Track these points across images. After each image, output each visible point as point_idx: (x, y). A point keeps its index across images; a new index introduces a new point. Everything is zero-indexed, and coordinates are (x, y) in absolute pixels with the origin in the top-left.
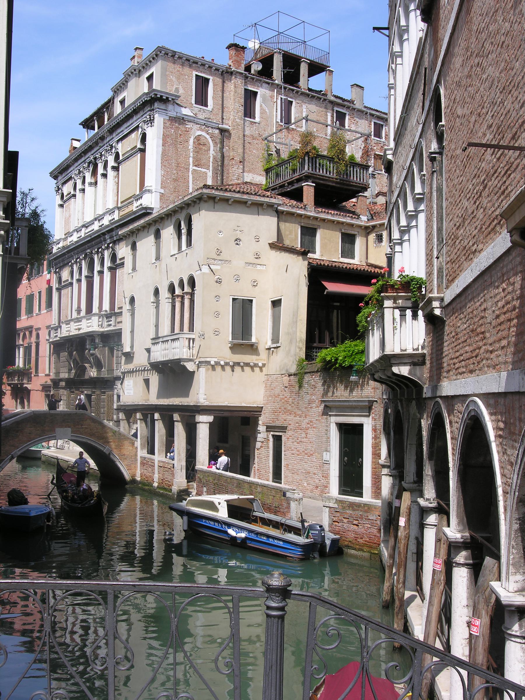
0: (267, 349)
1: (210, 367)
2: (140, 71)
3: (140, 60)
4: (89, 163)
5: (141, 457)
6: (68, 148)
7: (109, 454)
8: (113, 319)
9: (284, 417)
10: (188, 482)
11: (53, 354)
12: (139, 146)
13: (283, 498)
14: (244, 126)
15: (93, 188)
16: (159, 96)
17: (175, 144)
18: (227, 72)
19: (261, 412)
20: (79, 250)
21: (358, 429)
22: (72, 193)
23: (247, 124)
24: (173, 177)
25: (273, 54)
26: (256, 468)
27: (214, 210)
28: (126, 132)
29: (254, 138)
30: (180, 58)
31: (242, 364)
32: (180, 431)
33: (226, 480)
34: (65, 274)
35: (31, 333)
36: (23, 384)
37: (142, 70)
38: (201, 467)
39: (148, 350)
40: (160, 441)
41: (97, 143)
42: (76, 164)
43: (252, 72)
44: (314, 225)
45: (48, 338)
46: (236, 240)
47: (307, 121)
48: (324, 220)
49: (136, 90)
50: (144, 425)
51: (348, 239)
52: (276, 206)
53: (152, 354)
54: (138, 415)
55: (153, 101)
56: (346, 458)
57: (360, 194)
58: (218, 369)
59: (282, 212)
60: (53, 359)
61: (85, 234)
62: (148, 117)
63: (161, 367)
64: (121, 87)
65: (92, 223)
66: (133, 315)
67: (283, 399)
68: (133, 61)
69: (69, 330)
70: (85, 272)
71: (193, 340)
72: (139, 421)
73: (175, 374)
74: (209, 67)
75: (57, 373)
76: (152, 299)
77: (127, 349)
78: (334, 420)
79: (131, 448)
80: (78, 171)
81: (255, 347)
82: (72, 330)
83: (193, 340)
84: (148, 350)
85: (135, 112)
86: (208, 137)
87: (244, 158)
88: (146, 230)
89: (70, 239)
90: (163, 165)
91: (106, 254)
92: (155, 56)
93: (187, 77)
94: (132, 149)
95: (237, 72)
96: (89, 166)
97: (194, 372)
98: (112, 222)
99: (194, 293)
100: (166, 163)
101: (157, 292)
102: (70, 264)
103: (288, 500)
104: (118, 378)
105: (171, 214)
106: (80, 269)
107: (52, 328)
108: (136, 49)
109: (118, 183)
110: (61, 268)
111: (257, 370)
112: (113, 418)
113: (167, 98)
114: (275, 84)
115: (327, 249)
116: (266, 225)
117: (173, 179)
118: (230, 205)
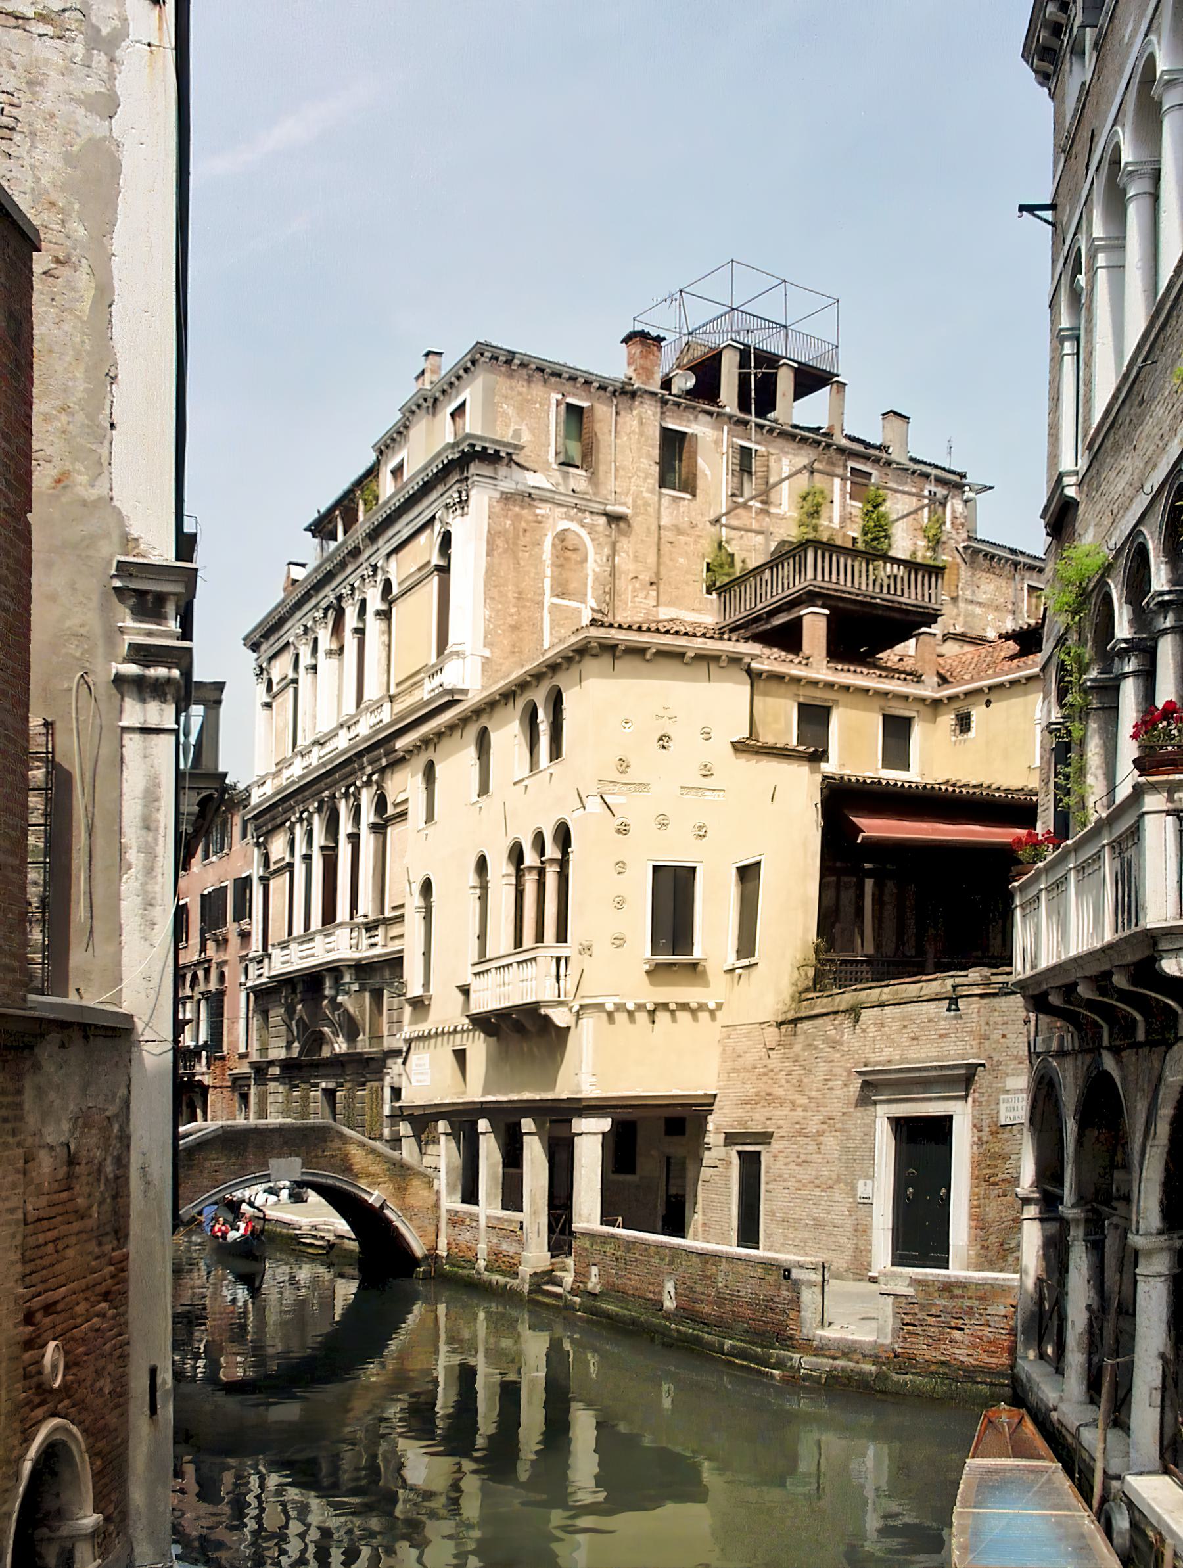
0: (725, 971)
1: (604, 1016)
2: (436, 400)
3: (435, 378)
4: (326, 609)
5: (448, 1211)
6: (281, 582)
7: (382, 1207)
8: (380, 931)
9: (766, 1112)
10: (552, 1257)
11: (254, 1012)
12: (436, 560)
13: (784, 1282)
14: (659, 505)
15: (334, 661)
16: (478, 448)
17: (512, 550)
18: (623, 392)
19: (712, 1104)
20: (307, 793)
21: (941, 1128)
22: (291, 675)
23: (665, 501)
24: (510, 621)
25: (720, 353)
26: (700, 1222)
27: (613, 674)
28: (405, 534)
29: (679, 531)
30: (523, 365)
31: (672, 1006)
32: (534, 1153)
33: (646, 1250)
34: (278, 847)
35: (207, 971)
36: (194, 1075)
37: (441, 398)
38: (585, 1225)
39: (465, 991)
40: (492, 1177)
41: (343, 565)
42: (299, 615)
43: (674, 391)
44: (826, 700)
45: (243, 980)
46: (661, 739)
47: (812, 472)
48: (847, 688)
49: (422, 450)
50: (453, 1145)
51: (897, 731)
52: (747, 660)
53: (472, 995)
54: (442, 1126)
55: (468, 460)
56: (911, 1190)
57: (924, 629)
58: (621, 1017)
59: (760, 674)
60: (254, 1023)
61: (320, 758)
62: (456, 495)
63: (489, 1024)
64: (393, 440)
65: (333, 734)
66: (428, 919)
67: (765, 1074)
68: (420, 380)
69: (288, 961)
70: (319, 839)
71: (567, 959)
72: (443, 1138)
73: (524, 1032)
74: (586, 382)
75: (264, 1050)
76: (473, 879)
77: (414, 989)
78: (883, 1113)
79: (426, 1193)
80: (302, 628)
81: (700, 968)
82: (294, 959)
83: (567, 959)
84: (465, 991)
85: (426, 488)
86: (583, 533)
87: (658, 573)
88: (457, 734)
89: (286, 773)
90: (488, 597)
91: (367, 797)
92: (469, 365)
93: (538, 406)
94: (420, 569)
95: (646, 392)
96: (325, 616)
97: (569, 1028)
98: (377, 728)
99: (568, 861)
100: (494, 593)
101: (482, 865)
102: (288, 824)
103: (796, 1286)
104: (396, 1053)
105: (514, 692)
106: (310, 834)
107: (252, 960)
108: (427, 354)
109: (389, 646)
110: (269, 834)
111: (704, 1016)
112: (381, 1134)
113: (497, 452)
114: (724, 414)
115: (856, 749)
116: (724, 703)
117: (510, 626)
118: (648, 661)
